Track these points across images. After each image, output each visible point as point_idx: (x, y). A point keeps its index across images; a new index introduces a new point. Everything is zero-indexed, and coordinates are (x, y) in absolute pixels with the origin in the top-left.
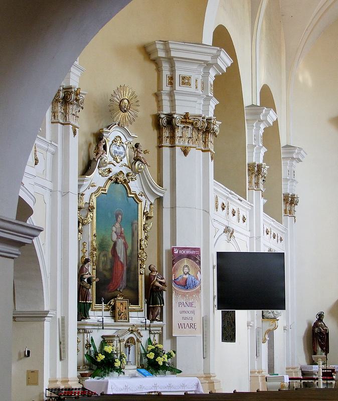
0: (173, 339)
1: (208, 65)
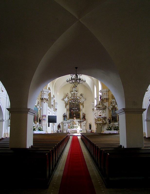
0: (42, 126)
1: (48, 92)
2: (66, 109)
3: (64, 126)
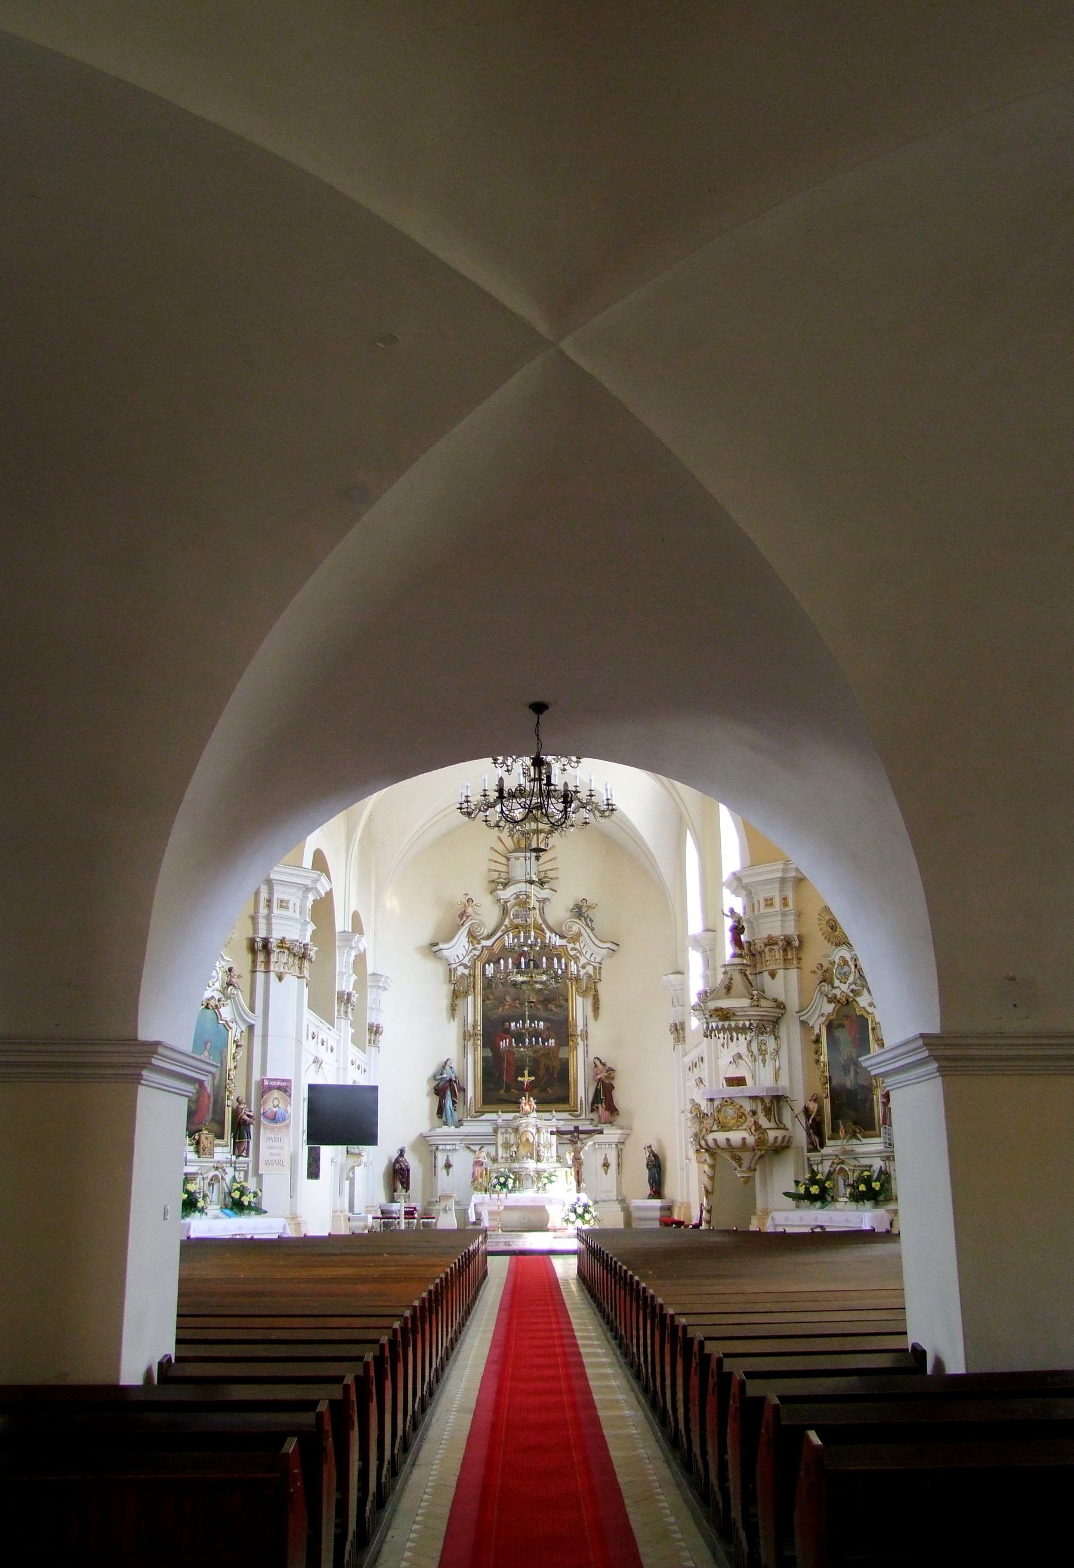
2: (451, 1032)
3: (441, 1172)
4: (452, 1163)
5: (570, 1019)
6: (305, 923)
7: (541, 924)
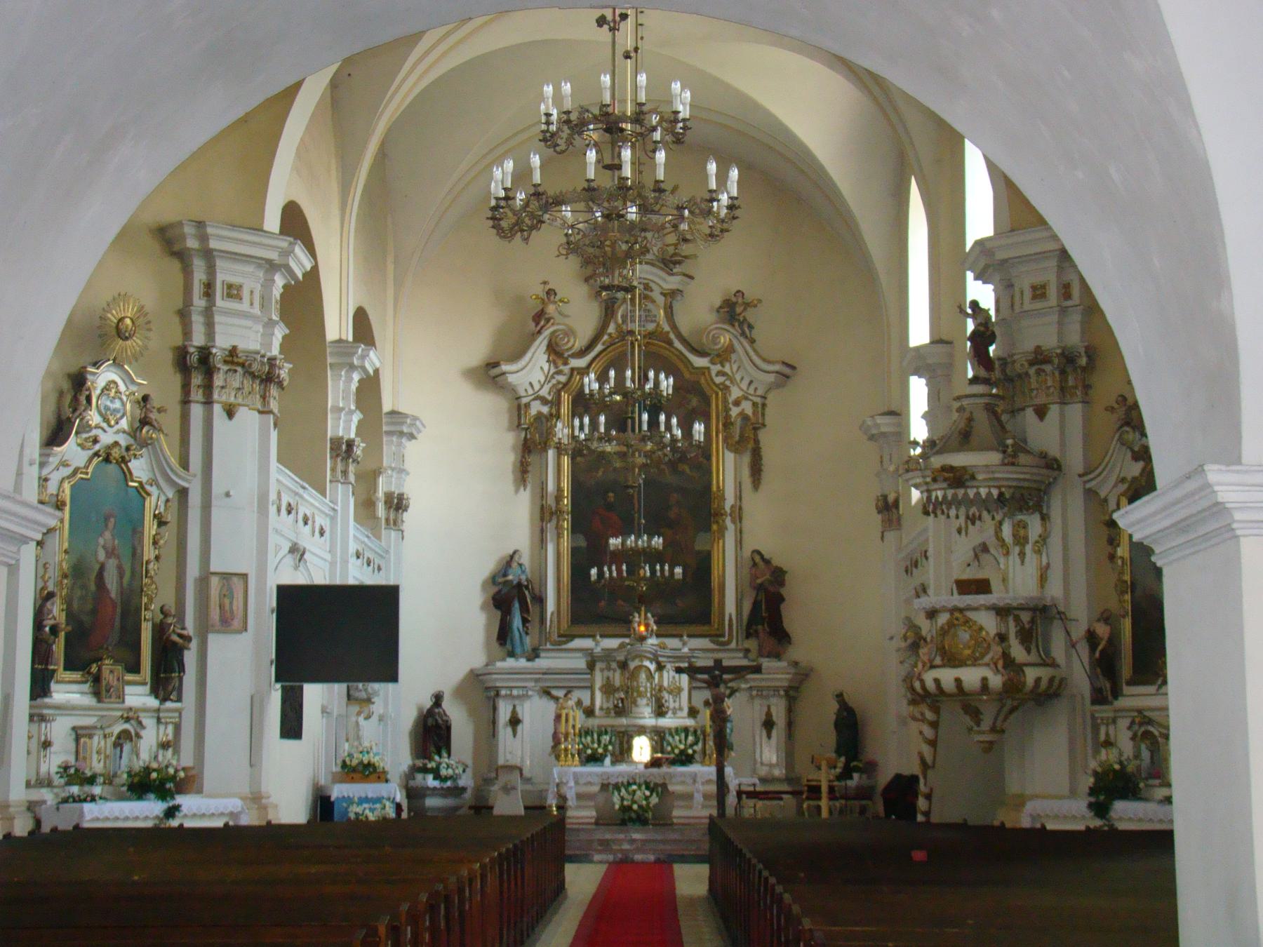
2: (521, 507)
3: (504, 732)
4: (521, 718)
5: (714, 488)
6: (270, 324)
7: (668, 333)
